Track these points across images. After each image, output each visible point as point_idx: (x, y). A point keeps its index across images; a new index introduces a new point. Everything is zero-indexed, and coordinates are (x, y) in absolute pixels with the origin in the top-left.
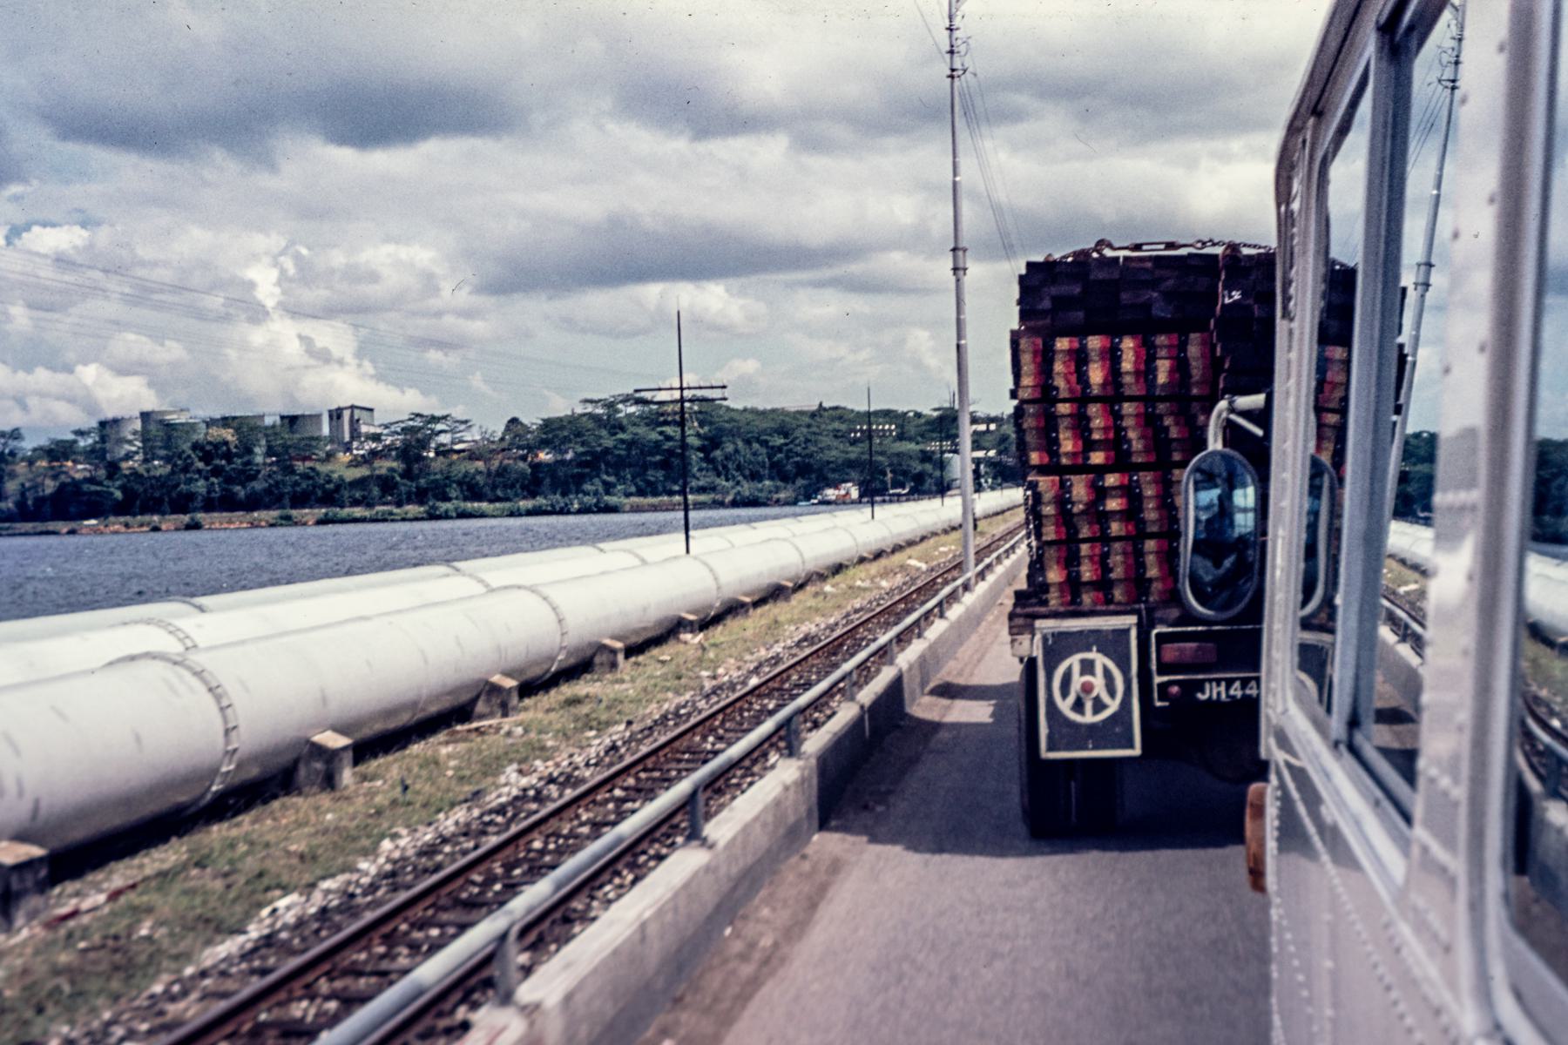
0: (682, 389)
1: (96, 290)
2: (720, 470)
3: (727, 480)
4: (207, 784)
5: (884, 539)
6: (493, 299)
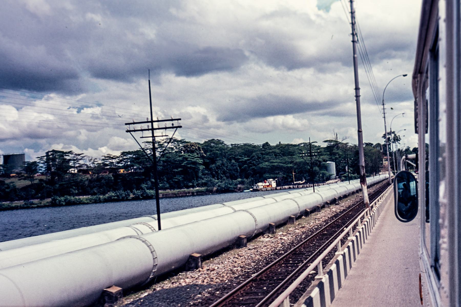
0: (153, 129)
1: (107, 125)
2: (215, 175)
3: (218, 179)
4: (148, 276)
5: (346, 191)
6: (224, 123)
